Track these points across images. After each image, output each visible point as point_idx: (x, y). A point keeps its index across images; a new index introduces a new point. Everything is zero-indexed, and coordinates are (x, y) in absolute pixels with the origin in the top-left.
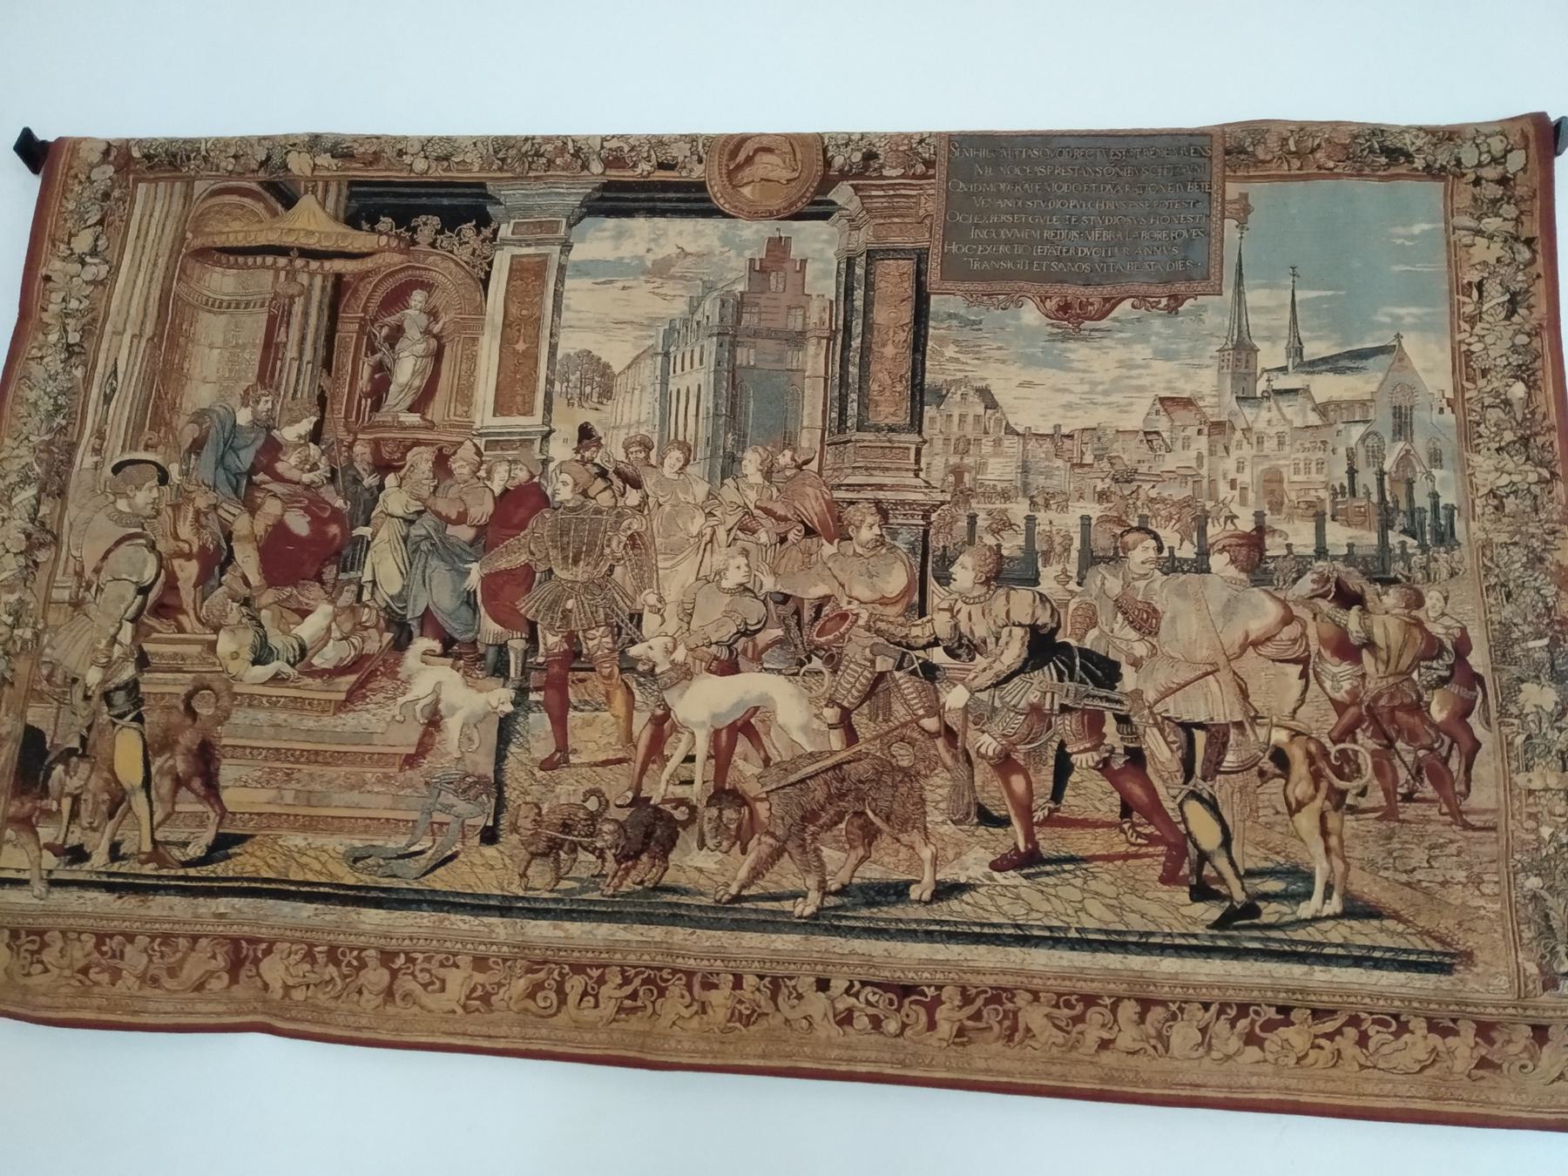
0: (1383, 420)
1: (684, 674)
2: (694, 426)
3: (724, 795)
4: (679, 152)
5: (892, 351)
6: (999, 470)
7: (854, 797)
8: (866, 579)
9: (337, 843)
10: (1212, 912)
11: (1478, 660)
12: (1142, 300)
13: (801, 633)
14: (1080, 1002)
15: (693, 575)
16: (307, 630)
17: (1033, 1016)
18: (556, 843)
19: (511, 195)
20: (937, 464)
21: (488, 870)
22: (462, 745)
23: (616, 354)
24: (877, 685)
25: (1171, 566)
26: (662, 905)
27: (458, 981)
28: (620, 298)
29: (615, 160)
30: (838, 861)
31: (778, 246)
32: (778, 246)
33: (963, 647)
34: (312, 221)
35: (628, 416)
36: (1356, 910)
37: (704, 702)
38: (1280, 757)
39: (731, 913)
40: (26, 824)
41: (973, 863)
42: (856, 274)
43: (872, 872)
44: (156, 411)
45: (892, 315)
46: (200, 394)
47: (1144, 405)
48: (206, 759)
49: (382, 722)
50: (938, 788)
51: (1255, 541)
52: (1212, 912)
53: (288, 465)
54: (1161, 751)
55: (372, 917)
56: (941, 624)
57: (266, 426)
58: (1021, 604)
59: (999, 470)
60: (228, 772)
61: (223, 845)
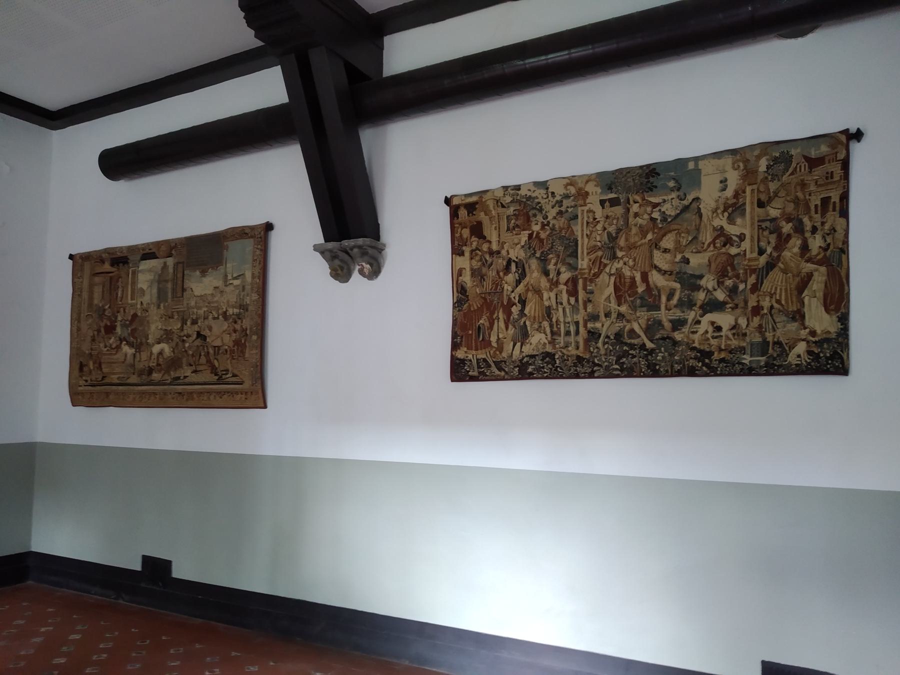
0: (241, 288)
1: (153, 345)
2: (155, 300)
3: (158, 365)
4: (151, 247)
5: (180, 282)
6: (193, 303)
7: (174, 363)
8: (175, 326)
9: (117, 376)
10: (217, 377)
11: (248, 332)
12: (213, 268)
13: (167, 336)
14: (201, 393)
15: (155, 328)
16: (111, 341)
17: (195, 396)
18: (141, 373)
19: (131, 258)
20: (185, 303)
21: (134, 379)
22: (130, 359)
23: (145, 288)
24: (177, 344)
25: (214, 318)
26: (150, 383)
27: (131, 396)
28: (146, 275)
29: (143, 250)
30: (173, 374)
31: (165, 263)
32: (165, 263)
33: (188, 336)
34: (107, 267)
35: (146, 299)
36: (234, 376)
37: (156, 349)
38: (226, 351)
39: (159, 383)
40: (81, 377)
41: (188, 373)
42: (176, 265)
43: (177, 375)
44: (90, 305)
45: (180, 275)
46: (96, 302)
47: (212, 288)
48: (100, 364)
49: (119, 356)
50: (184, 360)
51: (225, 313)
52: (217, 377)
53: (106, 313)
54: (211, 351)
55: (121, 388)
56: (185, 332)
57: (103, 306)
58: (196, 328)
59: (193, 303)
60: (103, 366)
61: (103, 378)
